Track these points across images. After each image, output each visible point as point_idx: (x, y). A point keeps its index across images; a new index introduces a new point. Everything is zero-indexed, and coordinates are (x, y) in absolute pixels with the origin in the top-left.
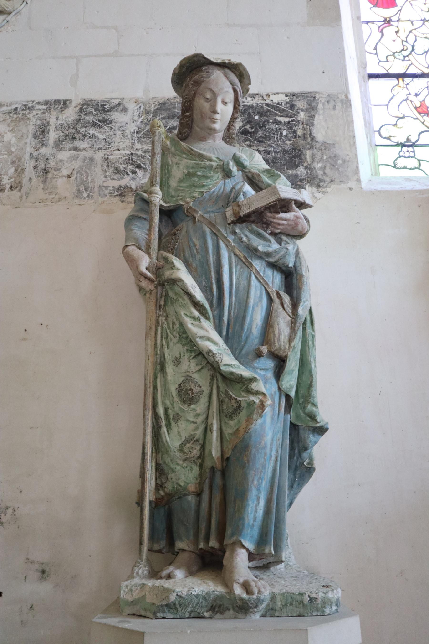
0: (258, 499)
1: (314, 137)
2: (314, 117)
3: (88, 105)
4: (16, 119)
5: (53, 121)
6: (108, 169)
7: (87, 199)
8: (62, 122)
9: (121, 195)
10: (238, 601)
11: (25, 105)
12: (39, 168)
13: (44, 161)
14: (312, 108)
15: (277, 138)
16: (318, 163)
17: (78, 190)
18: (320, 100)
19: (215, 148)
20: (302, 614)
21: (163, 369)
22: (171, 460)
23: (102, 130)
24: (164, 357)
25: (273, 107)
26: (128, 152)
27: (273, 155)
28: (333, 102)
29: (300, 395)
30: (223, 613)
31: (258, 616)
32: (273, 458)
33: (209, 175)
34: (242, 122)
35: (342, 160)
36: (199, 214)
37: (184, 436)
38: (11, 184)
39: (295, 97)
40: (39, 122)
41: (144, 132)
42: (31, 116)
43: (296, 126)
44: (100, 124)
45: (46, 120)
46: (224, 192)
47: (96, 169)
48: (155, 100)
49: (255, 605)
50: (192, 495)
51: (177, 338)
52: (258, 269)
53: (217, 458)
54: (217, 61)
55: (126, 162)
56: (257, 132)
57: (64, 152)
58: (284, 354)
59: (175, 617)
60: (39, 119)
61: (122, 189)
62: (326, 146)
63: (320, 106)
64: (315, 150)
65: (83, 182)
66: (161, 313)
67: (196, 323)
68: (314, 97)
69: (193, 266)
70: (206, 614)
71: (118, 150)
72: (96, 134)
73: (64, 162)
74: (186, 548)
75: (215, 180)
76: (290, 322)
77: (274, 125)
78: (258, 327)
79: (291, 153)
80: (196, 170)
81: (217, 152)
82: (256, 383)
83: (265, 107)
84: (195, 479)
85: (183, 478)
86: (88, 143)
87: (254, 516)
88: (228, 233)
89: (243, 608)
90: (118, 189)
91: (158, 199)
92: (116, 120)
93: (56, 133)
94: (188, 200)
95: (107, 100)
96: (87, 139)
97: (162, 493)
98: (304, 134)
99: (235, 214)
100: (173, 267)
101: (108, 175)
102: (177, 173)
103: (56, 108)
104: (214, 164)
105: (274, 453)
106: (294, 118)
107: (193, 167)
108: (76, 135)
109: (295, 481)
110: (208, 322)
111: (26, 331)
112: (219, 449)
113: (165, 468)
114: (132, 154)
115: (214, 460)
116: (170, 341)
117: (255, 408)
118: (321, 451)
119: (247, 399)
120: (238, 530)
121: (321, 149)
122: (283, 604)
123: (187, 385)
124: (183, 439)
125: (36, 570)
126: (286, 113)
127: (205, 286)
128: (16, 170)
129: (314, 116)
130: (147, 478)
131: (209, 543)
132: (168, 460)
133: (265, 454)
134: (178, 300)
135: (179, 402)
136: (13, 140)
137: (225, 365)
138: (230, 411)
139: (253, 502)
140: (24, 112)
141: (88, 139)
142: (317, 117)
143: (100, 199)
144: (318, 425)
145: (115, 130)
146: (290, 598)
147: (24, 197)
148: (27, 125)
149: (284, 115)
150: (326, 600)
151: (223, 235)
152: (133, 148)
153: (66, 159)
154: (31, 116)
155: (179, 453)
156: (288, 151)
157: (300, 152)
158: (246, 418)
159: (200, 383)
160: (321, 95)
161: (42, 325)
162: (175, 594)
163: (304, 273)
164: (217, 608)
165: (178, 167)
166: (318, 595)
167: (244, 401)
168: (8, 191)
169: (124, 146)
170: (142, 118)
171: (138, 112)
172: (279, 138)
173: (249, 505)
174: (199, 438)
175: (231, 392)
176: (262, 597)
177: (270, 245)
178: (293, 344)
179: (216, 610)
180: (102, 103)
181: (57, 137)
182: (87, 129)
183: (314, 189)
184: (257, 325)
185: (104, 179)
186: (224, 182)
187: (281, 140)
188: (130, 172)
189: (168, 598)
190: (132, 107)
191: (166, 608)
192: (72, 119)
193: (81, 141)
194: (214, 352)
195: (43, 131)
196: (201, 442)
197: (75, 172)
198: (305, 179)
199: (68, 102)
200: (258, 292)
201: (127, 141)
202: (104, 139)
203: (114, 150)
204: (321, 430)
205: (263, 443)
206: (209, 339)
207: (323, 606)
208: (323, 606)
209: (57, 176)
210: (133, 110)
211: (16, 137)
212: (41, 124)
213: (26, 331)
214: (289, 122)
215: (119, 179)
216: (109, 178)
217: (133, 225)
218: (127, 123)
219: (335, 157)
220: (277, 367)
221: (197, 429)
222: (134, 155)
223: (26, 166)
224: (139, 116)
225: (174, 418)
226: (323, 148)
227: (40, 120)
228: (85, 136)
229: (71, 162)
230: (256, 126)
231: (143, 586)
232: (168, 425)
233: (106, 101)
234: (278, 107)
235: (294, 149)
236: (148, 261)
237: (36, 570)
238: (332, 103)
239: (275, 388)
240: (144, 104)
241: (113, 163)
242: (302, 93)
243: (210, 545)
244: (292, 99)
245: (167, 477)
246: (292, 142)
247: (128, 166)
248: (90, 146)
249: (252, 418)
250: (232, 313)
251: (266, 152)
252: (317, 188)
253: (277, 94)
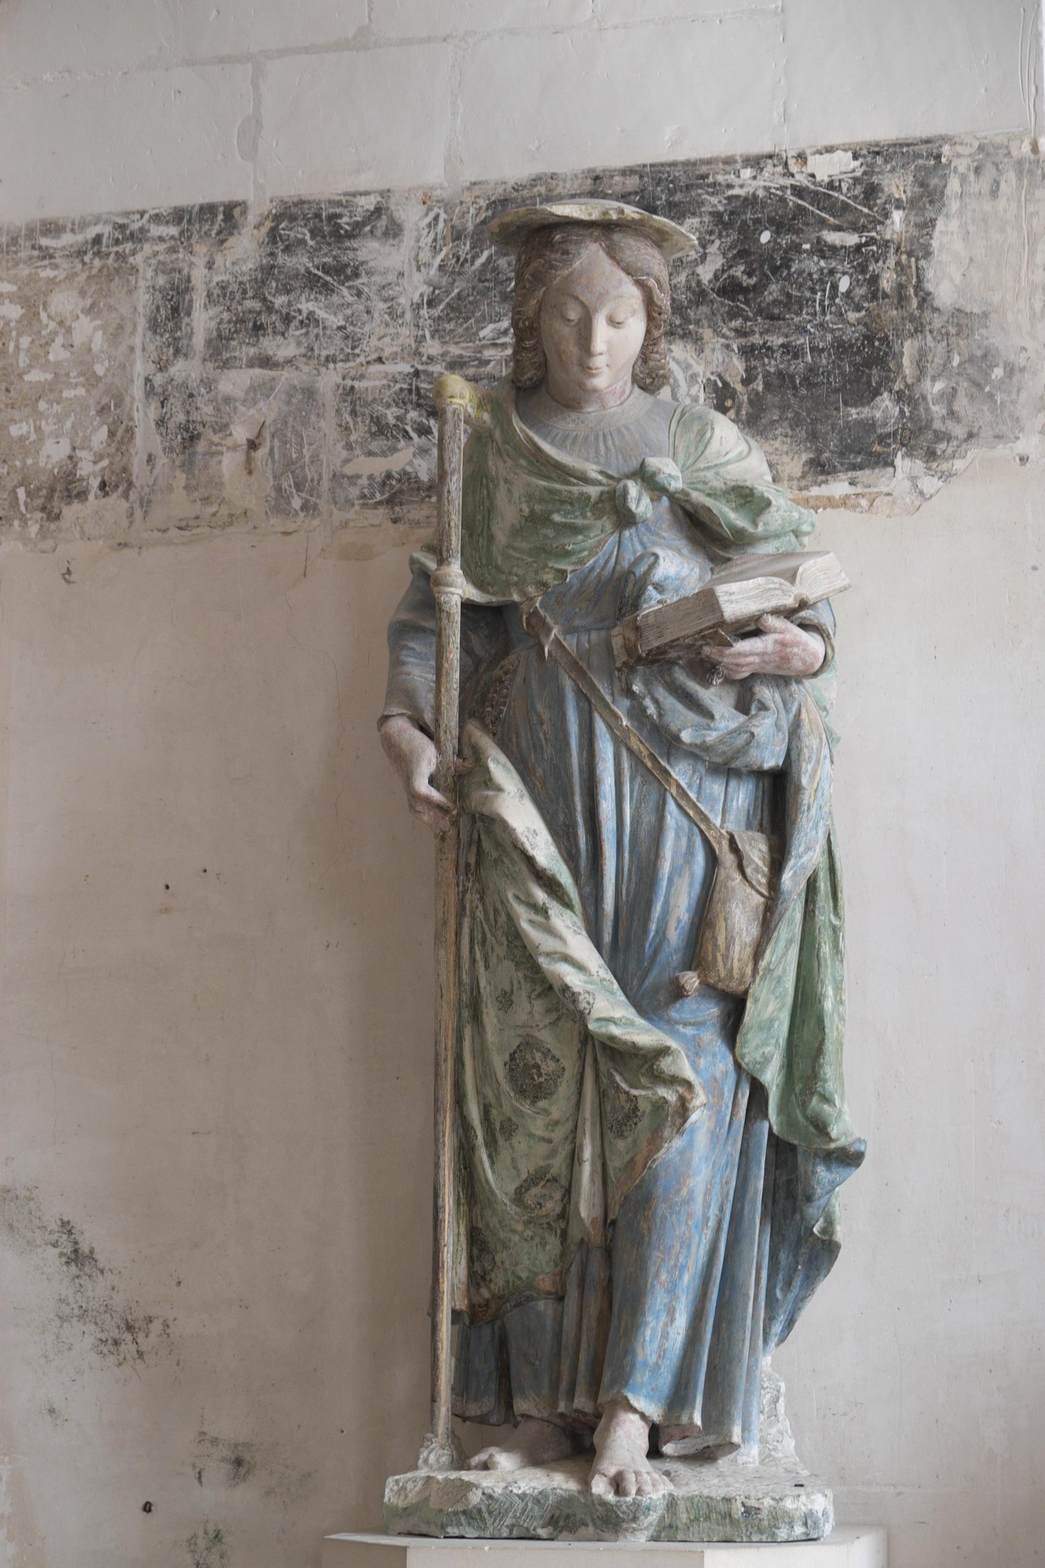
0: (671, 1312)
1: (929, 294)
2: (934, 226)
3: (293, 219)
4: (100, 270)
5: (199, 275)
6: (355, 423)
7: (302, 514)
8: (225, 278)
9: (390, 502)
10: (598, 1507)
11: (122, 227)
12: (171, 425)
13: (184, 402)
14: (930, 194)
15: (822, 301)
16: (934, 379)
17: (279, 489)
18: (953, 165)
19: (601, 434)
20: (729, 1538)
21: (477, 1017)
22: (500, 1222)
23: (335, 298)
24: (479, 988)
25: (816, 198)
26: (407, 368)
27: (809, 358)
28: (994, 171)
29: (797, 1074)
30: (575, 1532)
31: (641, 1539)
32: (712, 1223)
33: (579, 522)
34: (724, 254)
35: (1006, 365)
36: (552, 636)
37: (526, 1170)
38: (103, 477)
39: (879, 160)
40: (161, 281)
41: (447, 300)
42: (138, 260)
43: (877, 261)
44: (328, 279)
45: (180, 272)
46: (618, 568)
47: (322, 424)
48: (477, 191)
49: (631, 1516)
50: (546, 1299)
51: (505, 948)
52: (683, 784)
53: (592, 1222)
54: (590, 215)
55: (400, 401)
56: (766, 287)
57: (233, 374)
58: (742, 988)
59: (482, 1535)
60: (161, 268)
61: (394, 482)
62: (962, 321)
63: (954, 185)
64: (929, 338)
65: (289, 464)
66: (470, 885)
67: (539, 919)
68: (938, 157)
69: (538, 775)
70: (542, 1532)
71: (380, 360)
72: (318, 311)
73: (237, 404)
74: (534, 1412)
75: (597, 536)
76: (761, 909)
77: (815, 258)
78: (682, 924)
79: (859, 352)
80: (550, 506)
81: (607, 447)
82: (671, 1058)
83: (791, 199)
84: (552, 1263)
85: (525, 1261)
86: (299, 344)
87: (660, 1347)
88: (616, 692)
89: (608, 1522)
90: (383, 484)
91: (458, 589)
92: (371, 264)
93: (212, 312)
94: (531, 590)
95: (344, 199)
96: (295, 332)
97: (485, 1293)
98: (901, 287)
99: (630, 649)
100: (489, 782)
101: (356, 442)
102: (508, 511)
103: (205, 233)
104: (593, 491)
105: (713, 1212)
106: (873, 234)
107: (541, 500)
108: (263, 318)
109: (796, 1269)
110: (569, 912)
111: (167, 887)
112: (598, 1200)
113: (490, 1240)
114: (417, 374)
115: (584, 1225)
116: (490, 951)
117: (667, 1115)
118: (849, 1203)
119: (649, 1093)
120: (623, 1377)
121: (948, 334)
122: (692, 1517)
123: (528, 1057)
124: (524, 1176)
125: (223, 1460)
126: (850, 217)
127: (564, 824)
128: (112, 434)
129: (933, 222)
130: (443, 1262)
131: (573, 1401)
132: (494, 1221)
133: (690, 1215)
134: (502, 862)
135: (512, 1094)
136: (98, 341)
137: (599, 1020)
138: (618, 1119)
139: (657, 1318)
140: (120, 248)
141: (297, 329)
142: (940, 224)
143: (338, 516)
144: (833, 1146)
145: (368, 299)
146: (705, 1506)
147: (139, 513)
148: (130, 292)
149: (845, 225)
150: (779, 1512)
151: (603, 699)
152: (420, 354)
153: (240, 394)
154: (138, 260)
155: (514, 1207)
156: (851, 346)
157: (884, 347)
158: (649, 1135)
159: (556, 1053)
160: (959, 149)
161: (205, 871)
162: (479, 1492)
163: (804, 781)
164: (564, 1521)
165: (509, 491)
166: (762, 1504)
167: (645, 1097)
168: (96, 497)
169: (395, 349)
170: (442, 255)
171: (432, 236)
172: (826, 303)
173: (646, 1324)
174: (559, 1175)
175: (621, 1074)
176: (645, 1500)
177: (712, 725)
178: (763, 964)
179: (561, 1524)
180: (331, 211)
181: (213, 324)
182: (293, 296)
183: (919, 465)
184: (679, 921)
185: (345, 454)
186: (620, 537)
187: (833, 309)
188: (414, 430)
189: (467, 1500)
190: (412, 216)
191: (463, 1518)
192: (251, 266)
193: (279, 337)
194: (576, 990)
195: (173, 306)
196: (564, 1182)
197: (267, 434)
198: (895, 433)
199: (236, 213)
200: (684, 841)
201: (404, 331)
202: (341, 328)
203: (368, 363)
204: (849, 1158)
205: (684, 1192)
206: (567, 959)
207: (772, 1524)
208: (772, 1524)
209: (219, 448)
210: (418, 230)
211: (104, 328)
212: (168, 286)
213: (167, 887)
214: (858, 247)
215: (383, 454)
216: (358, 452)
217: (405, 647)
218: (401, 274)
219: (986, 358)
220: (729, 1015)
221: (553, 1154)
222: (422, 377)
223: (136, 419)
224: (435, 250)
225: (502, 1128)
226: (953, 330)
227: (163, 272)
228: (287, 319)
229: (255, 402)
230: (762, 266)
231: (427, 1481)
232: (491, 1144)
233: (339, 204)
234: (830, 196)
235: (869, 338)
236: (434, 761)
237: (223, 1460)
238: (989, 172)
239: (724, 1064)
240: (448, 207)
241: (366, 404)
242: (901, 145)
243: (574, 1406)
244: (871, 165)
245: (494, 1259)
246: (863, 313)
247: (407, 411)
248: (303, 350)
249: (661, 1136)
250: (624, 891)
251: (788, 352)
252: (927, 462)
253: (830, 150)
